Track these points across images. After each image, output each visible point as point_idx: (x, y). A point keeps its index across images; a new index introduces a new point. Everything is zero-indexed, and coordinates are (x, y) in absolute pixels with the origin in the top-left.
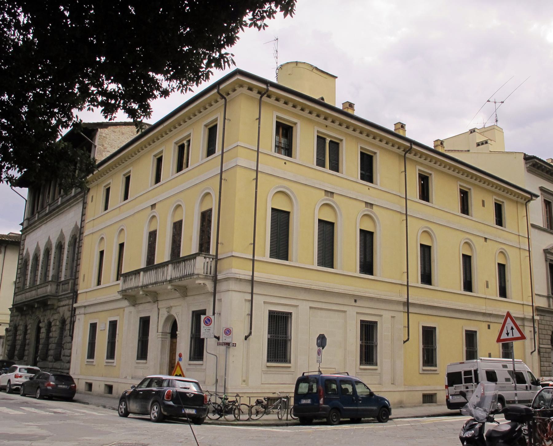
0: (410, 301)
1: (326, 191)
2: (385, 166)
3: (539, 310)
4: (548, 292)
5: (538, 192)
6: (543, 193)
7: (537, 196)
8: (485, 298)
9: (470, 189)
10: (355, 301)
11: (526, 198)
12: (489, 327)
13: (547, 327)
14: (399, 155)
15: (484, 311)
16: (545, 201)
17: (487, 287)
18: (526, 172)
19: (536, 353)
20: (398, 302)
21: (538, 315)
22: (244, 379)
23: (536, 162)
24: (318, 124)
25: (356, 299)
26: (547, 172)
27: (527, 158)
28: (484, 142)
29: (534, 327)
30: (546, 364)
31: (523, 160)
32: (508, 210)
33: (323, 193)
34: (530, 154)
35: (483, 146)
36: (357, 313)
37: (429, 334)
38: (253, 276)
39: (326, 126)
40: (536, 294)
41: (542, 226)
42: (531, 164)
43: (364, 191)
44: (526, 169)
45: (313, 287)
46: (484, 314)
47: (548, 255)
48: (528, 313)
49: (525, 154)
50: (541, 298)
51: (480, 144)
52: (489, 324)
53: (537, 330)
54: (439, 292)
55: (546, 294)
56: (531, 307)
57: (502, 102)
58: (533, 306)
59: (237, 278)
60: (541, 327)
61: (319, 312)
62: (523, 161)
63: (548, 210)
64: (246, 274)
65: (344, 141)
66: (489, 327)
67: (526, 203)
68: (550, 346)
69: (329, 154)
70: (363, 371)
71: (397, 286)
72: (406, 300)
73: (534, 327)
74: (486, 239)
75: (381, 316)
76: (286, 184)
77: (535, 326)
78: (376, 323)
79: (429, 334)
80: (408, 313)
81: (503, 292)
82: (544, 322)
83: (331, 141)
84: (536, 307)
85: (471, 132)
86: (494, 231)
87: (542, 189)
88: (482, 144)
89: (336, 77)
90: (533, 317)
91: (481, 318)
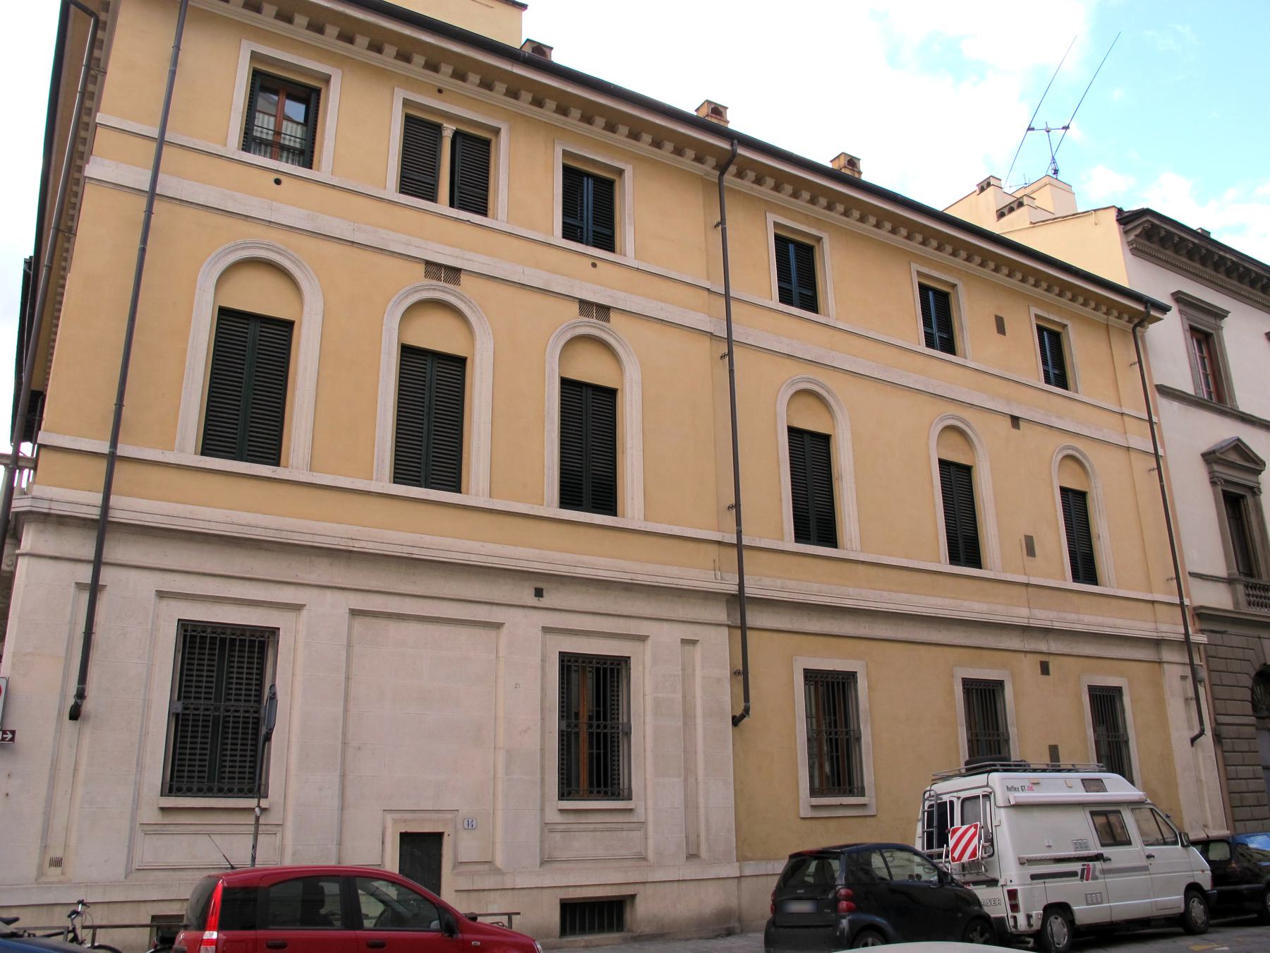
0: (749, 591)
1: (428, 263)
2: (656, 213)
3: (1204, 616)
4: (1228, 568)
5: (1166, 300)
6: (1183, 308)
7: (1164, 309)
8: (1027, 585)
9: (954, 286)
10: (539, 593)
11: (1133, 313)
12: (1045, 669)
13: (1235, 666)
14: (705, 182)
15: (1024, 622)
16: (1193, 330)
17: (1031, 551)
18: (1130, 255)
19: (1208, 736)
20: (708, 596)
21: (1202, 631)
22: (57, 853)
23: (1153, 225)
24: (408, 82)
25: (540, 583)
26: (1190, 255)
27: (1125, 219)
28: (1015, 205)
29: (1192, 664)
30: (1245, 771)
31: (1115, 225)
32: (1082, 348)
33: (421, 268)
34: (1130, 206)
35: (1014, 214)
36: (546, 630)
37: (831, 696)
38: (105, 507)
39: (440, 91)
40: (1191, 574)
41: (1191, 391)
42: (1138, 231)
43: (581, 272)
44: (1127, 249)
45: (357, 546)
46: (1026, 630)
47: (1216, 468)
48: (1171, 627)
49: (1120, 211)
50: (1209, 585)
51: (1006, 211)
52: (1044, 658)
53: (1203, 674)
54: (861, 568)
55: (1222, 572)
56: (1179, 610)
57: (1066, 128)
58: (1182, 605)
59: (48, 515)
60: (1216, 664)
61: (393, 628)
62: (1115, 228)
63: (1205, 354)
64: (86, 501)
65: (503, 134)
66: (1045, 669)
67: (1136, 326)
68: (1252, 720)
69: (444, 165)
70: (571, 818)
71: (703, 546)
72: (734, 589)
73: (1192, 664)
74: (1015, 421)
75: (642, 639)
76: (275, 237)
77: (1197, 661)
78: (626, 660)
79: (831, 696)
80: (743, 628)
81: (1084, 566)
82: (1223, 652)
83: (457, 134)
84: (1195, 609)
85: (982, 189)
86: (1042, 403)
87: (1179, 297)
88: (1011, 210)
89: (524, 7)
90: (1187, 634)
91: (1014, 642)
